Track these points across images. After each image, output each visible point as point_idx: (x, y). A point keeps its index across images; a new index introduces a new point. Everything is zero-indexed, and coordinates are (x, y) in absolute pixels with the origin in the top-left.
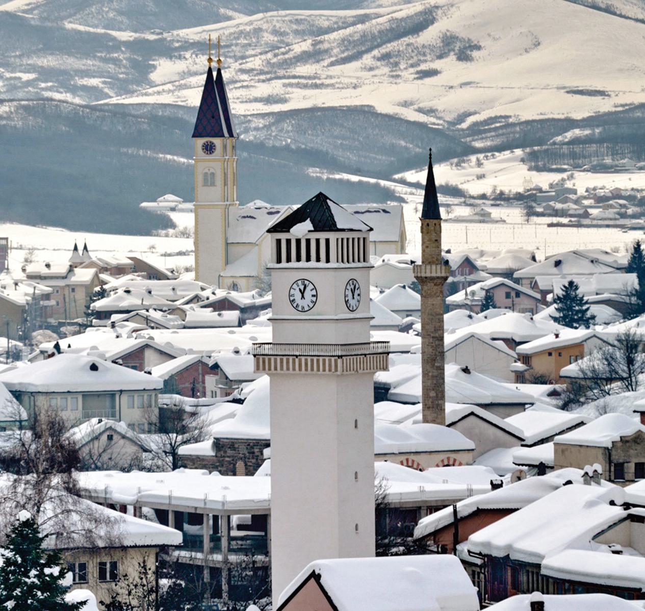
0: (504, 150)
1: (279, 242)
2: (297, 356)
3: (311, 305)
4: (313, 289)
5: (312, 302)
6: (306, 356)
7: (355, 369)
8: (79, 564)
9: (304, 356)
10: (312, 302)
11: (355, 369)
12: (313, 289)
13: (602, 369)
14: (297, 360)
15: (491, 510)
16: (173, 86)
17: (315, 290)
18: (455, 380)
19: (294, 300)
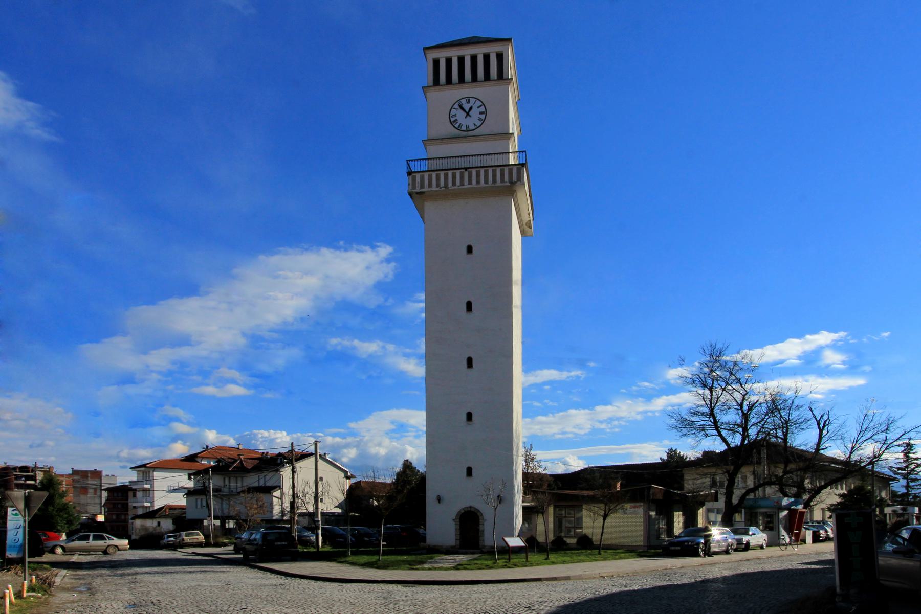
0: (739, 501)
1: (436, 63)
2: (466, 169)
3: (478, 123)
4: (481, 106)
5: (480, 119)
6: (437, 170)
7: (442, 184)
8: (321, 513)
9: (442, 170)
10: (480, 119)
11: (442, 184)
12: (481, 106)
13: (339, 511)
14: (466, 174)
15: (529, 190)
16: (916, 471)
17: (483, 106)
18: (646, 499)
19: (456, 120)
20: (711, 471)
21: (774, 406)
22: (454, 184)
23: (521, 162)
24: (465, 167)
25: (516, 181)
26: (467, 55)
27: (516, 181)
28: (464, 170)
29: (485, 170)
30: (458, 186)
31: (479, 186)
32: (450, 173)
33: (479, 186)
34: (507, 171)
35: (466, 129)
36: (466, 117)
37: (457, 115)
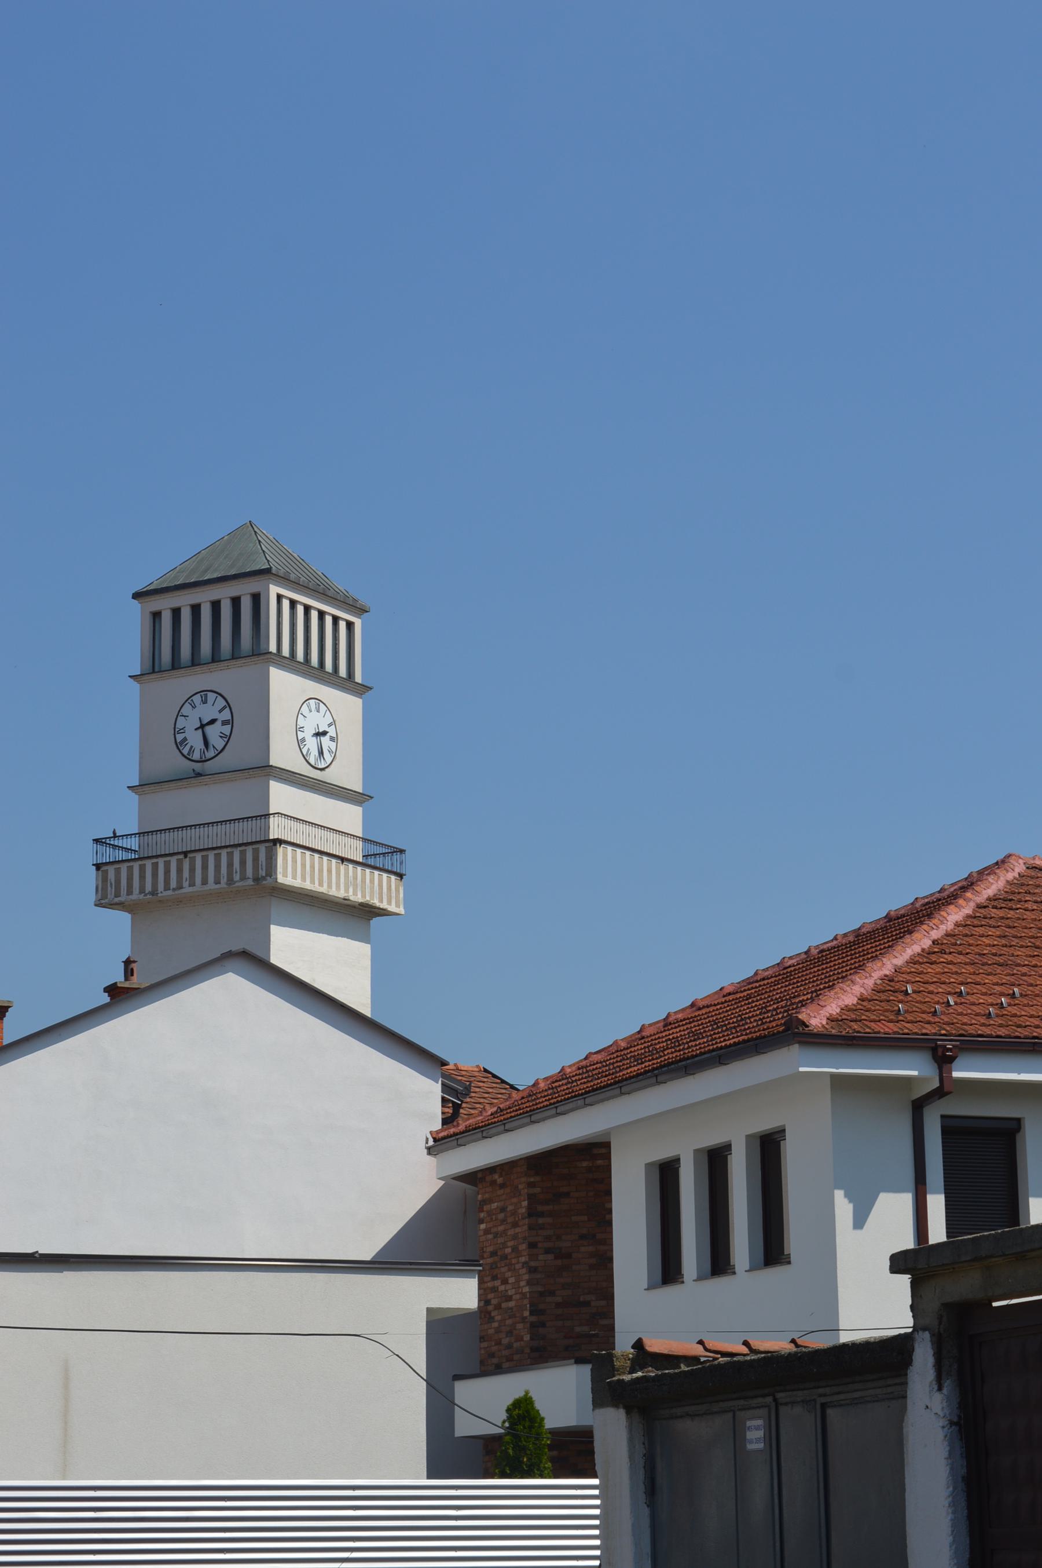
2: (185, 854)
11: (148, 888)
19: (185, 739)
20: (917, 949)
21: (999, 877)
22: (167, 887)
23: (184, 850)
24: (184, 850)
25: (264, 875)
26: (164, 609)
27: (264, 875)
28: (181, 857)
29: (202, 856)
30: (174, 890)
31: (206, 888)
32: (161, 862)
33: (206, 888)
34: (251, 853)
35: (201, 758)
36: (196, 729)
37: (306, 739)
